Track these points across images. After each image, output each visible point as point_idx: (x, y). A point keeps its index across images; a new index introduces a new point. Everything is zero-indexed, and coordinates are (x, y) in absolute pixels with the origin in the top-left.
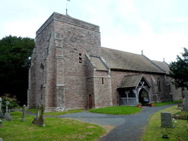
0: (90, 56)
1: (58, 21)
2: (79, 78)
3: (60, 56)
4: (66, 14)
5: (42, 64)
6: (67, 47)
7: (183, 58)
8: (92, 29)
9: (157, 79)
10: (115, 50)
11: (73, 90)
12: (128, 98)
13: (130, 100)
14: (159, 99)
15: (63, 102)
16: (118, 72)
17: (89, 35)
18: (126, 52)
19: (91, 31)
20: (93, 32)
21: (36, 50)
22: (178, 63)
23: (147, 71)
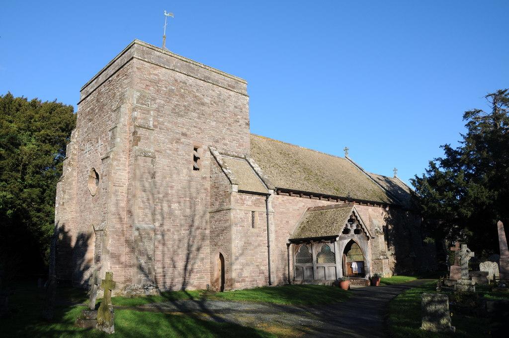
1: (145, 63)
20: (232, 93)
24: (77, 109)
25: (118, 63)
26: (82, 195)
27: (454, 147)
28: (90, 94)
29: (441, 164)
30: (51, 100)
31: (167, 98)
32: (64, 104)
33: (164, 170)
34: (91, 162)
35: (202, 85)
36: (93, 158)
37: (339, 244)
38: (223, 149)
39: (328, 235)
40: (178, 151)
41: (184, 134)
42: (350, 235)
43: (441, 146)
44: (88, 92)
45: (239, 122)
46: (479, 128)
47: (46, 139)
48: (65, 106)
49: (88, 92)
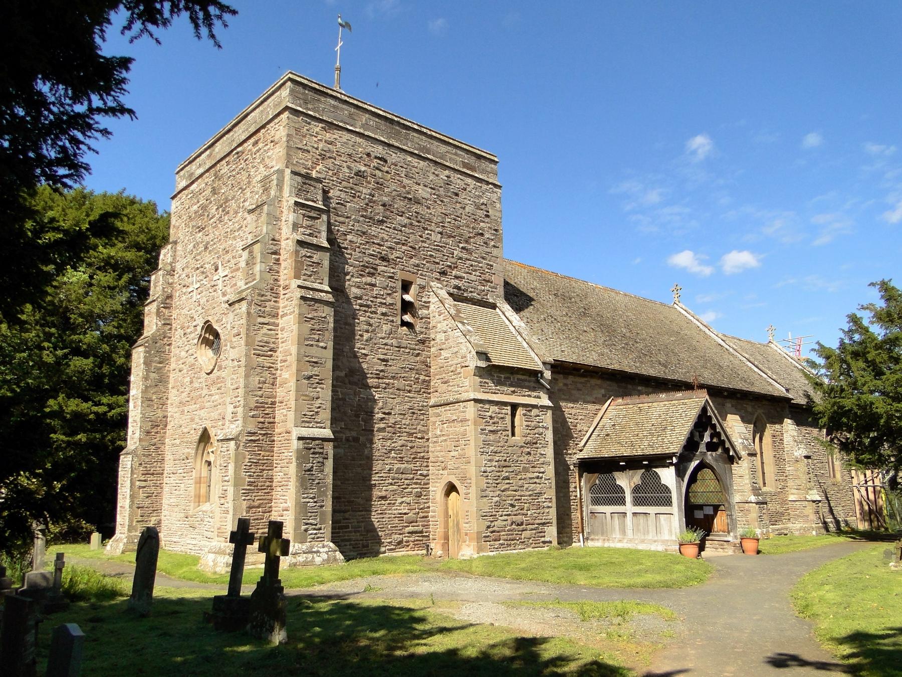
0: (451, 295)
7: (878, 331)
12: (629, 507)
13: (641, 519)
16: (583, 380)
21: (174, 257)
26: (185, 371)
29: (873, 317)
30: (113, 191)
36: (208, 301)
39: (656, 452)
43: (872, 284)
44: (192, 174)
49: (192, 174)
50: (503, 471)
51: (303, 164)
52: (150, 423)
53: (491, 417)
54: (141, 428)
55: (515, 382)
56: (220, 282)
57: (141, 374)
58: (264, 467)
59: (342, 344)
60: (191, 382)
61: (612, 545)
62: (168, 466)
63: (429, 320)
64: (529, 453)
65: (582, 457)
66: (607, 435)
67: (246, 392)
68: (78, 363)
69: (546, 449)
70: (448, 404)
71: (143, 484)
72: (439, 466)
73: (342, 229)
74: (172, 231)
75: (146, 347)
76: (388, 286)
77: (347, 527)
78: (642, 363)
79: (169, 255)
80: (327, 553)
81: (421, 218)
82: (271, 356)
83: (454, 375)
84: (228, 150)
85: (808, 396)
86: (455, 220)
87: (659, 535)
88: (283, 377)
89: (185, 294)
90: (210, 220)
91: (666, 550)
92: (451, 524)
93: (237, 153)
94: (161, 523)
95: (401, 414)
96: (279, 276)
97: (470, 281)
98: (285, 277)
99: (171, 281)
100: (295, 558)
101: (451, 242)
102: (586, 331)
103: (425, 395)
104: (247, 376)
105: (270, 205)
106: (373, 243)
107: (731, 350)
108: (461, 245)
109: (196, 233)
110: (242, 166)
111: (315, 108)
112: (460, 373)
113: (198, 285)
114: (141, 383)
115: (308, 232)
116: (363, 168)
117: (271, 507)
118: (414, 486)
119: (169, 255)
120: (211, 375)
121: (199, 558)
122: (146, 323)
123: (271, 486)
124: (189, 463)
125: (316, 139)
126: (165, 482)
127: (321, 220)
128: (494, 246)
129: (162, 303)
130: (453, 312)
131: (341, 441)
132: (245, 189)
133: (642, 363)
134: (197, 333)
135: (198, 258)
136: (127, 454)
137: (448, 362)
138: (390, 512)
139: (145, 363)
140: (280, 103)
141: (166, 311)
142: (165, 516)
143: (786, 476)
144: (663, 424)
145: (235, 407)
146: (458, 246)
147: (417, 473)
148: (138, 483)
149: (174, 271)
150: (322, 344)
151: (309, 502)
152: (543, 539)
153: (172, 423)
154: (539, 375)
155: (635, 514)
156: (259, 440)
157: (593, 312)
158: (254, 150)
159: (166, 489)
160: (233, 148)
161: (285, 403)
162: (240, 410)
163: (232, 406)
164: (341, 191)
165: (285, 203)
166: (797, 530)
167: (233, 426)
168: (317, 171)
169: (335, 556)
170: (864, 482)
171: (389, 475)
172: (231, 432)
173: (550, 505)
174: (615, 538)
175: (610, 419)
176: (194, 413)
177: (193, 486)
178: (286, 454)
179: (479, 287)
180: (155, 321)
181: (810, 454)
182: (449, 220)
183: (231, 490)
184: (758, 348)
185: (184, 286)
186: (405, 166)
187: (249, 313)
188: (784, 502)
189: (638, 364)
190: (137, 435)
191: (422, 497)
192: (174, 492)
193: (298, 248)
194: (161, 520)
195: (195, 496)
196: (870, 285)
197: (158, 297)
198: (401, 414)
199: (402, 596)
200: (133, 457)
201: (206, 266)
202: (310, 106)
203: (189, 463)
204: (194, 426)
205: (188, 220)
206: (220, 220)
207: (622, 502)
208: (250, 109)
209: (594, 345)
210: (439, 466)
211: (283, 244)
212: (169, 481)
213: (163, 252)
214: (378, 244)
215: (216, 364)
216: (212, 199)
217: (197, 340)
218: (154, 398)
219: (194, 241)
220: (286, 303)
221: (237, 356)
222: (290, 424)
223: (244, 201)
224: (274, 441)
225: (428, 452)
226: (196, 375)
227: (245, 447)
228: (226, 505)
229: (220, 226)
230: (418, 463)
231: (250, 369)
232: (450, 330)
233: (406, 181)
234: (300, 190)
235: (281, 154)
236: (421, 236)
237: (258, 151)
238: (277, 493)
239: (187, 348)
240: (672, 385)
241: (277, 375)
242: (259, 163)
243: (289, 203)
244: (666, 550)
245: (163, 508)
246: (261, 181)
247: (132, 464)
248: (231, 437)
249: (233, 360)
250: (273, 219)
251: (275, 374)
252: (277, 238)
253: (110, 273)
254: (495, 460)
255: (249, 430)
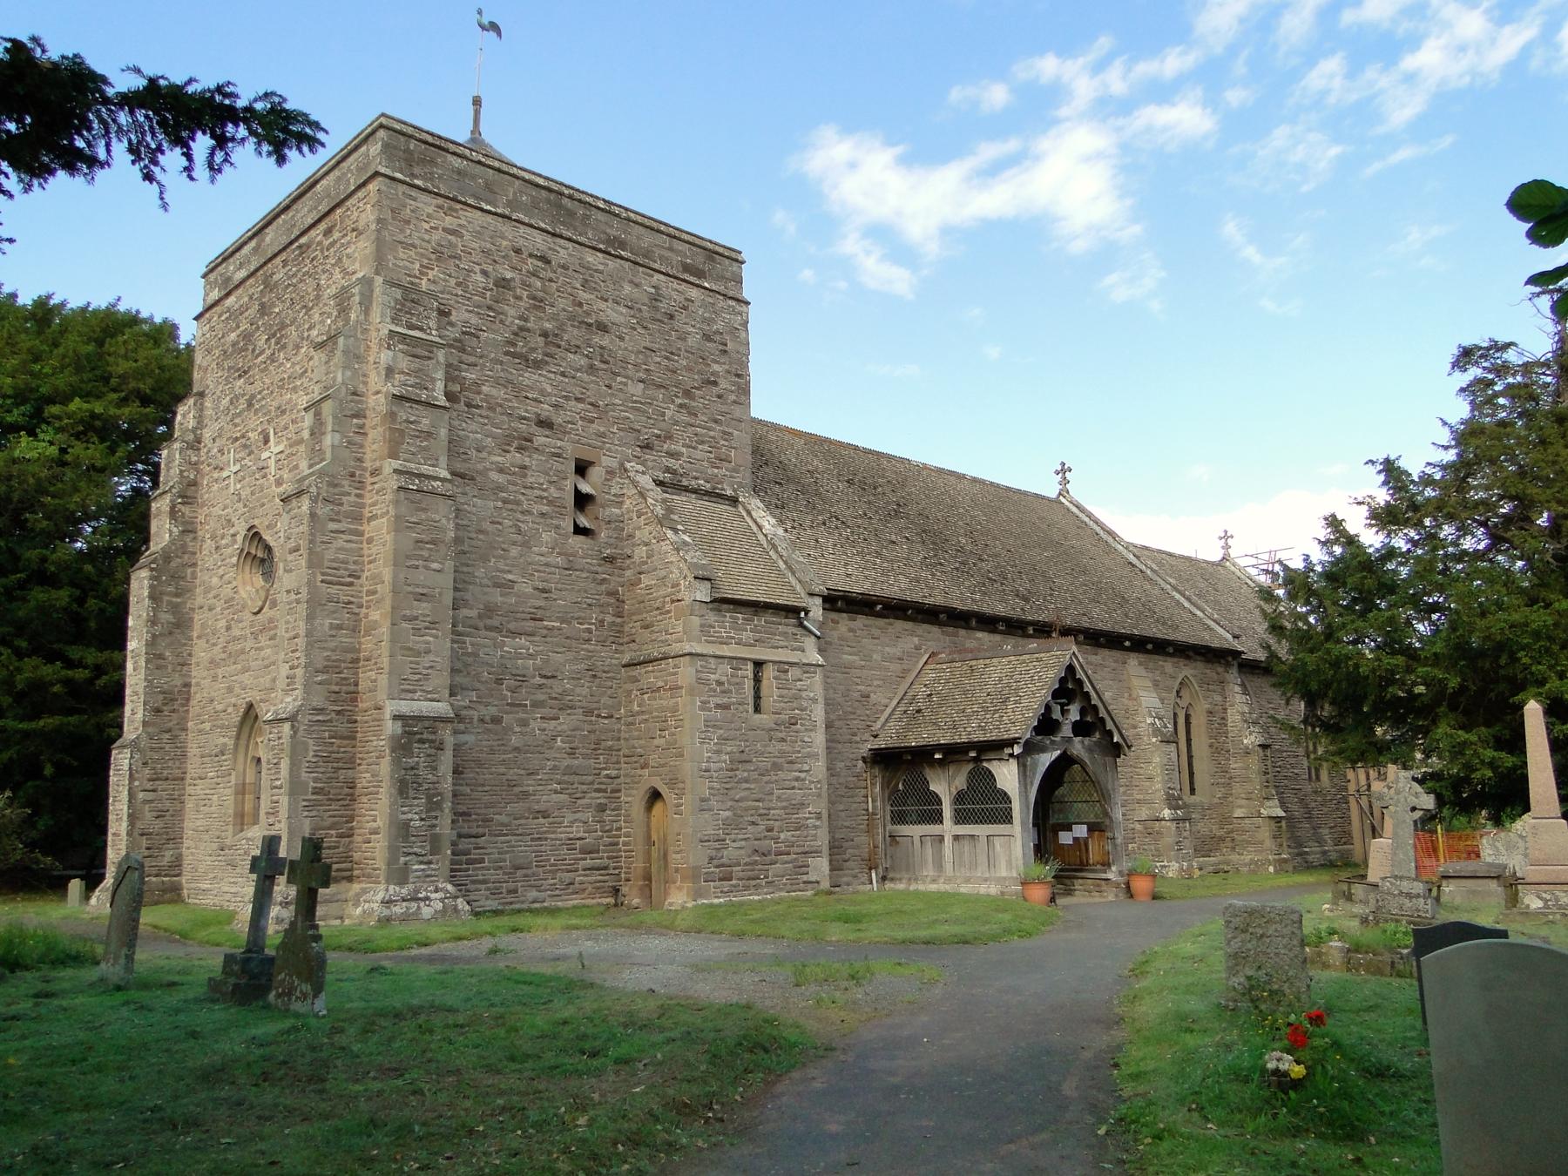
0: (659, 483)
1: (414, 193)
2: (570, 655)
3: (419, 476)
4: (468, 135)
5: (255, 536)
6: (478, 400)
7: (1372, 540)
8: (686, 268)
9: (1168, 689)
10: (856, 448)
11: (516, 749)
12: (948, 827)
13: (966, 846)
14: (1187, 843)
15: (435, 850)
16: (881, 622)
17: (661, 316)
18: (940, 471)
19: (675, 284)
20: (694, 293)
21: (200, 419)
22: (1334, 575)
23: (1101, 626)
24: (188, 333)
25: (327, 189)
27: (1414, 466)
28: (237, 287)
30: (100, 301)
31: (489, 308)
32: (144, 314)
33: (481, 532)
34: (245, 506)
35: (601, 267)
36: (252, 493)
37: (1025, 766)
38: (667, 470)
40: (525, 476)
41: (545, 424)
42: (1057, 739)
43: (1372, 462)
45: (715, 383)
46: (1501, 401)
47: (95, 428)
48: (149, 321)
50: (737, 769)
51: (406, 268)
52: (161, 697)
53: (719, 683)
54: (145, 704)
55: (763, 626)
56: (272, 463)
57: (145, 614)
58: (340, 765)
59: (473, 565)
60: (228, 628)
61: (921, 887)
62: (193, 768)
63: (621, 525)
64: (783, 740)
65: (877, 747)
66: (919, 711)
67: (308, 644)
68: (42, 596)
69: (813, 734)
70: (651, 662)
71: (150, 796)
72: (636, 762)
73: (473, 376)
74: (196, 376)
75: (152, 570)
76: (551, 469)
77: (482, 861)
78: (985, 594)
79: (191, 415)
80: (442, 900)
81: (610, 356)
82: (351, 584)
83: (661, 614)
84: (285, 240)
85: (1268, 647)
86: (667, 358)
87: (992, 870)
88: (370, 618)
89: (216, 481)
90: (256, 358)
91: (1003, 893)
92: (654, 855)
93: (300, 247)
94: (181, 860)
95: (573, 678)
96: (364, 453)
97: (694, 460)
98: (375, 455)
99: (194, 459)
100: (388, 908)
101: (661, 396)
102: (894, 543)
103: (614, 646)
104: (310, 618)
105: (347, 337)
106: (527, 398)
107: (1149, 572)
108: (679, 401)
109: (234, 379)
110: (306, 269)
111: (426, 173)
112: (669, 612)
113: (238, 467)
114: (145, 630)
115: (412, 381)
116: (509, 275)
117: (352, 828)
118: (594, 794)
119: (191, 415)
120: (259, 616)
121: (237, 913)
122: (153, 529)
123: (352, 795)
124: (226, 761)
125: (426, 226)
126: (188, 792)
127: (434, 361)
128: (735, 402)
129: (180, 496)
130: (659, 510)
131: (470, 723)
132: (311, 308)
133: (985, 594)
134: (236, 547)
135: (237, 421)
136: (124, 747)
137: (651, 594)
138: (553, 836)
139: (152, 597)
140: (367, 165)
141: (186, 510)
142: (188, 848)
143: (1231, 778)
144: (1004, 693)
145: (292, 668)
146: (673, 402)
147: (600, 774)
148: (141, 795)
149: (199, 443)
150: (435, 566)
151: (411, 820)
152: (805, 878)
153: (198, 696)
154: (802, 614)
155: (956, 838)
156: (330, 721)
157: (912, 510)
158: (326, 243)
159: (189, 805)
160: (293, 237)
161: (373, 661)
162: (299, 672)
163: (287, 666)
164: (471, 311)
165: (374, 334)
166: (1245, 865)
167: (289, 699)
168: (429, 280)
169: (456, 906)
170: (1366, 787)
171: (552, 777)
172: (285, 708)
173: (818, 823)
174: (927, 876)
175: (925, 685)
176: (233, 678)
177: (233, 797)
178: (375, 743)
179: (709, 471)
180: (168, 526)
181: (1269, 742)
182: (659, 359)
183: (284, 801)
184: (1202, 568)
185: (215, 469)
186: (582, 270)
187: (313, 515)
188: (1226, 820)
189: (978, 597)
190: (140, 716)
191: (608, 812)
192: (202, 808)
193: (394, 409)
194: (181, 855)
195: (236, 815)
196: (1367, 463)
197: (172, 487)
198: (573, 678)
199: (543, 959)
200: (132, 751)
201: (250, 434)
202: (416, 170)
203: (226, 761)
204: (233, 700)
205: (222, 357)
206: (272, 358)
207: (937, 818)
208: (322, 171)
209: (905, 565)
210: (636, 762)
211: (372, 401)
212: (195, 791)
213: (181, 409)
214: (535, 400)
215: (267, 598)
216: (260, 323)
217: (236, 558)
218: (167, 654)
219: (230, 393)
220: (376, 498)
221: (294, 585)
222: (381, 696)
223: (309, 329)
224: (356, 722)
225: (619, 739)
226: (236, 617)
227: (308, 732)
228: (277, 826)
229: (271, 368)
230: (601, 757)
231: (315, 605)
232: (654, 541)
233: (583, 296)
234: (399, 310)
235: (367, 251)
236: (609, 387)
237: (332, 244)
238: (363, 805)
239: (221, 571)
240: (1034, 630)
241: (361, 616)
242: (333, 265)
243: (381, 333)
244: (1003, 893)
245: (185, 836)
246: (335, 296)
247: (130, 764)
248: (284, 716)
249: (288, 592)
250: (355, 357)
251: (357, 614)
252: (361, 388)
253: (93, 443)
254: (724, 751)
255: (315, 704)
